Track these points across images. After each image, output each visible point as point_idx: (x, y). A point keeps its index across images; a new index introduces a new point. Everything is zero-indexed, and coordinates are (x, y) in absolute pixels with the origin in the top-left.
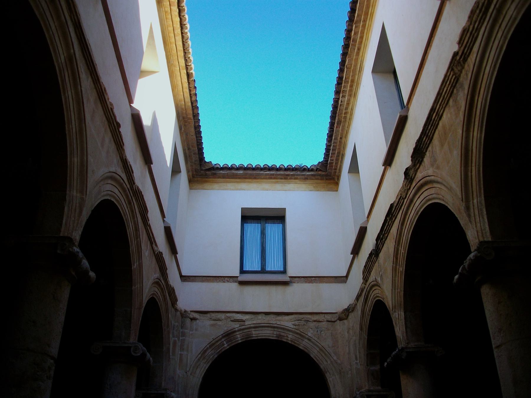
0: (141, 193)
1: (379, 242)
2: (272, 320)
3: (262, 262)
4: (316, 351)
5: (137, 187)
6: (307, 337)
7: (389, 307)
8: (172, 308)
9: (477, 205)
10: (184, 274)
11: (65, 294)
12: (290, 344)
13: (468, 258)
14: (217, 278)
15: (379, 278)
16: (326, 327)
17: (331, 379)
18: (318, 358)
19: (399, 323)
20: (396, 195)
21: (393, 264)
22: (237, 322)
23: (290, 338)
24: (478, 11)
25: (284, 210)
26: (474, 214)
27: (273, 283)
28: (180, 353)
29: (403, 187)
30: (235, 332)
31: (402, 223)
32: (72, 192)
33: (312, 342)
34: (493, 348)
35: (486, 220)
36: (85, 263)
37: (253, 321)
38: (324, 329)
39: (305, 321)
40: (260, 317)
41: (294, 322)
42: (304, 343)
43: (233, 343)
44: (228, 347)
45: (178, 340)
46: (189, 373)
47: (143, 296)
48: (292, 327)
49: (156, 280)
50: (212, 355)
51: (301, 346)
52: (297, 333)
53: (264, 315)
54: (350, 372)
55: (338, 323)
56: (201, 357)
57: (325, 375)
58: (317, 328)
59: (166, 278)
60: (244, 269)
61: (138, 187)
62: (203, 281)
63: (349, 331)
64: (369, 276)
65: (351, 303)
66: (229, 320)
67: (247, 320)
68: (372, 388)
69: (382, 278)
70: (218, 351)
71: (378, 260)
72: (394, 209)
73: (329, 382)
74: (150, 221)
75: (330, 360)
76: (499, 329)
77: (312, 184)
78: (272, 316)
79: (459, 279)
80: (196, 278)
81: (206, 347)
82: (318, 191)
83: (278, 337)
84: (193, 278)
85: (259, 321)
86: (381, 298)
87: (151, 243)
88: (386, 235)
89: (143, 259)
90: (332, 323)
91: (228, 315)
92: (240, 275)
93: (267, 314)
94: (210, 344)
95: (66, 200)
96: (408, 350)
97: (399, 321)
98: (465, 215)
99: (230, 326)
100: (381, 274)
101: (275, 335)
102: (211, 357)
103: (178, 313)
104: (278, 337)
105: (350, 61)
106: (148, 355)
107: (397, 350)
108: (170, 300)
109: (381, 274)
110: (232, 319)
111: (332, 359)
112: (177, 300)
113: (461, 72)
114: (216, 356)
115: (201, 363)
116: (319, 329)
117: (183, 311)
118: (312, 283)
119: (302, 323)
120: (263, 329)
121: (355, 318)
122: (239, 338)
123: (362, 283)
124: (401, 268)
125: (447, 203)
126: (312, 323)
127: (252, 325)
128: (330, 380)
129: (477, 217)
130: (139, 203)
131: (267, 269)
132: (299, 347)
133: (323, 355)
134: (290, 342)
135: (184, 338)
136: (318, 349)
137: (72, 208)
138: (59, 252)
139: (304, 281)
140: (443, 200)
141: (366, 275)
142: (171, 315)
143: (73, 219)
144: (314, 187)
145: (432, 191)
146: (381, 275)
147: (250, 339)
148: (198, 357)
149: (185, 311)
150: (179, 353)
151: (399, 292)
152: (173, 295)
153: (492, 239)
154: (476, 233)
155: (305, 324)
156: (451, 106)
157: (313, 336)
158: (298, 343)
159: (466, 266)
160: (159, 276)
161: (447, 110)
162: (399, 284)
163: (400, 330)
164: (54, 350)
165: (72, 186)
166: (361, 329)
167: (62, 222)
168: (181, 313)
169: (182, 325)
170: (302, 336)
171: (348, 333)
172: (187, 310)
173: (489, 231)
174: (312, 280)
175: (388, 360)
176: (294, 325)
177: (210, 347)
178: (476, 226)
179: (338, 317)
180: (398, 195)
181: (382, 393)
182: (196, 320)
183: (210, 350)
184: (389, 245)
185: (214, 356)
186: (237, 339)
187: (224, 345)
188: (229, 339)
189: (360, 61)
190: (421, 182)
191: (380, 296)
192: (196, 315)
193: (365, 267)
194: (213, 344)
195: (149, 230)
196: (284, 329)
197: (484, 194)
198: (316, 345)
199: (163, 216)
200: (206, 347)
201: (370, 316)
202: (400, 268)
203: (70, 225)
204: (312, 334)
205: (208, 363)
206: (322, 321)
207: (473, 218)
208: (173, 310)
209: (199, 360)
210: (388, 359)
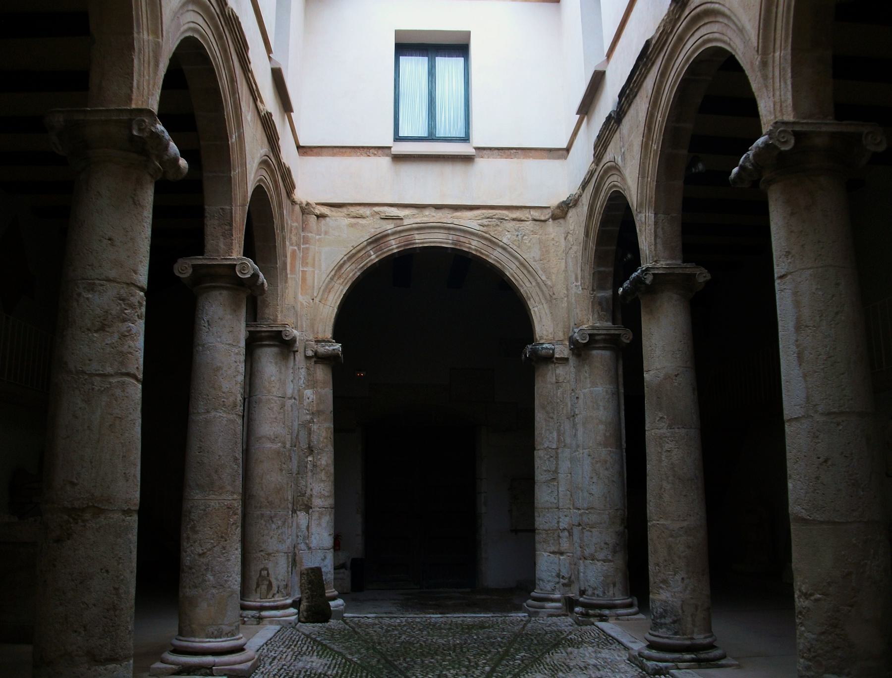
0: (236, 19)
1: (624, 99)
2: (446, 217)
3: (430, 123)
5: (230, 10)
6: (501, 244)
7: (632, 205)
8: (288, 201)
9: (778, 61)
10: (301, 144)
11: (148, 197)
12: (474, 254)
13: (755, 145)
14: (356, 150)
15: (620, 157)
17: (536, 309)
18: (517, 278)
19: (645, 230)
20: (657, 27)
21: (643, 137)
22: (391, 221)
23: (473, 245)
25: (468, 34)
26: (773, 75)
27: (448, 158)
28: (302, 269)
29: (668, 14)
30: (387, 235)
31: (663, 74)
32: (142, 34)
33: (509, 253)
34: (775, 278)
35: (790, 87)
36: (173, 148)
39: (499, 219)
40: (427, 212)
41: (480, 221)
43: (385, 253)
44: (377, 260)
45: (299, 250)
46: (317, 300)
47: (248, 185)
48: (478, 228)
49: (263, 158)
50: (352, 272)
53: (433, 210)
54: (566, 299)
56: (335, 274)
57: (527, 303)
59: (278, 153)
60: (401, 134)
61: (232, 10)
62: (334, 155)
63: (567, 236)
64: (603, 153)
65: (572, 193)
66: (378, 217)
67: (407, 216)
68: (597, 325)
69: (624, 157)
70: (361, 265)
71: (620, 129)
72: (650, 50)
73: (532, 313)
74: (252, 64)
75: (536, 280)
76: (786, 252)
79: (738, 173)
80: (323, 150)
81: (343, 260)
84: (319, 150)
85: (425, 219)
86: (621, 189)
87: (255, 100)
88: (636, 90)
89: (244, 125)
90: (542, 223)
91: (376, 209)
92: (393, 144)
94: (348, 256)
95: (134, 49)
96: (656, 272)
97: (645, 227)
98: (759, 74)
99: (379, 226)
100: (623, 151)
102: (351, 275)
103: (297, 208)
104: (456, 244)
106: (261, 274)
107: (639, 271)
108: (284, 188)
109: (623, 151)
110: (383, 215)
111: (539, 279)
112: (294, 187)
114: (359, 274)
115: (336, 284)
117: (304, 203)
118: (512, 158)
119: (494, 222)
120: (433, 231)
121: (577, 219)
122: (394, 246)
123: (591, 163)
124: (655, 144)
125: (735, 51)
126: (509, 222)
127: (414, 226)
128: (534, 310)
129: (777, 80)
130: (234, 34)
131: (438, 134)
133: (525, 272)
134: (474, 252)
135: (307, 246)
136: (517, 264)
137: (144, 61)
138: (135, 133)
139: (499, 155)
140: (729, 45)
141: (600, 150)
142: (286, 210)
143: (147, 77)
145: (715, 28)
146: (624, 153)
147: (411, 247)
148: (330, 276)
149: (308, 204)
150: (301, 269)
151: (649, 182)
152: (288, 180)
153: (794, 118)
154: (772, 106)
155: (499, 223)
157: (510, 243)
158: (486, 253)
159: (751, 156)
160: (268, 151)
162: (650, 170)
163: (645, 241)
164: (143, 279)
165: (141, 24)
166: (587, 234)
167: (132, 84)
168: (301, 207)
169: (303, 226)
170: (493, 243)
171: (565, 239)
172: (310, 202)
173: (791, 105)
175: (625, 285)
176: (481, 225)
177: (350, 258)
178: (773, 95)
179: (550, 214)
180: (659, 27)
181: (613, 332)
182: (326, 217)
183: (349, 264)
184: (640, 107)
185: (354, 275)
186: (391, 248)
187: (371, 256)
188: (379, 247)
190: (698, 10)
191: (619, 185)
192: (325, 210)
193: (599, 137)
194: (354, 255)
195: (251, 78)
197: (792, 46)
199: (269, 50)
200: (343, 260)
201: (601, 215)
202: (653, 145)
203: (144, 88)
204: (509, 239)
205: (346, 284)
206: (526, 219)
207: (771, 81)
208: (289, 202)
209: (332, 279)
210: (625, 283)
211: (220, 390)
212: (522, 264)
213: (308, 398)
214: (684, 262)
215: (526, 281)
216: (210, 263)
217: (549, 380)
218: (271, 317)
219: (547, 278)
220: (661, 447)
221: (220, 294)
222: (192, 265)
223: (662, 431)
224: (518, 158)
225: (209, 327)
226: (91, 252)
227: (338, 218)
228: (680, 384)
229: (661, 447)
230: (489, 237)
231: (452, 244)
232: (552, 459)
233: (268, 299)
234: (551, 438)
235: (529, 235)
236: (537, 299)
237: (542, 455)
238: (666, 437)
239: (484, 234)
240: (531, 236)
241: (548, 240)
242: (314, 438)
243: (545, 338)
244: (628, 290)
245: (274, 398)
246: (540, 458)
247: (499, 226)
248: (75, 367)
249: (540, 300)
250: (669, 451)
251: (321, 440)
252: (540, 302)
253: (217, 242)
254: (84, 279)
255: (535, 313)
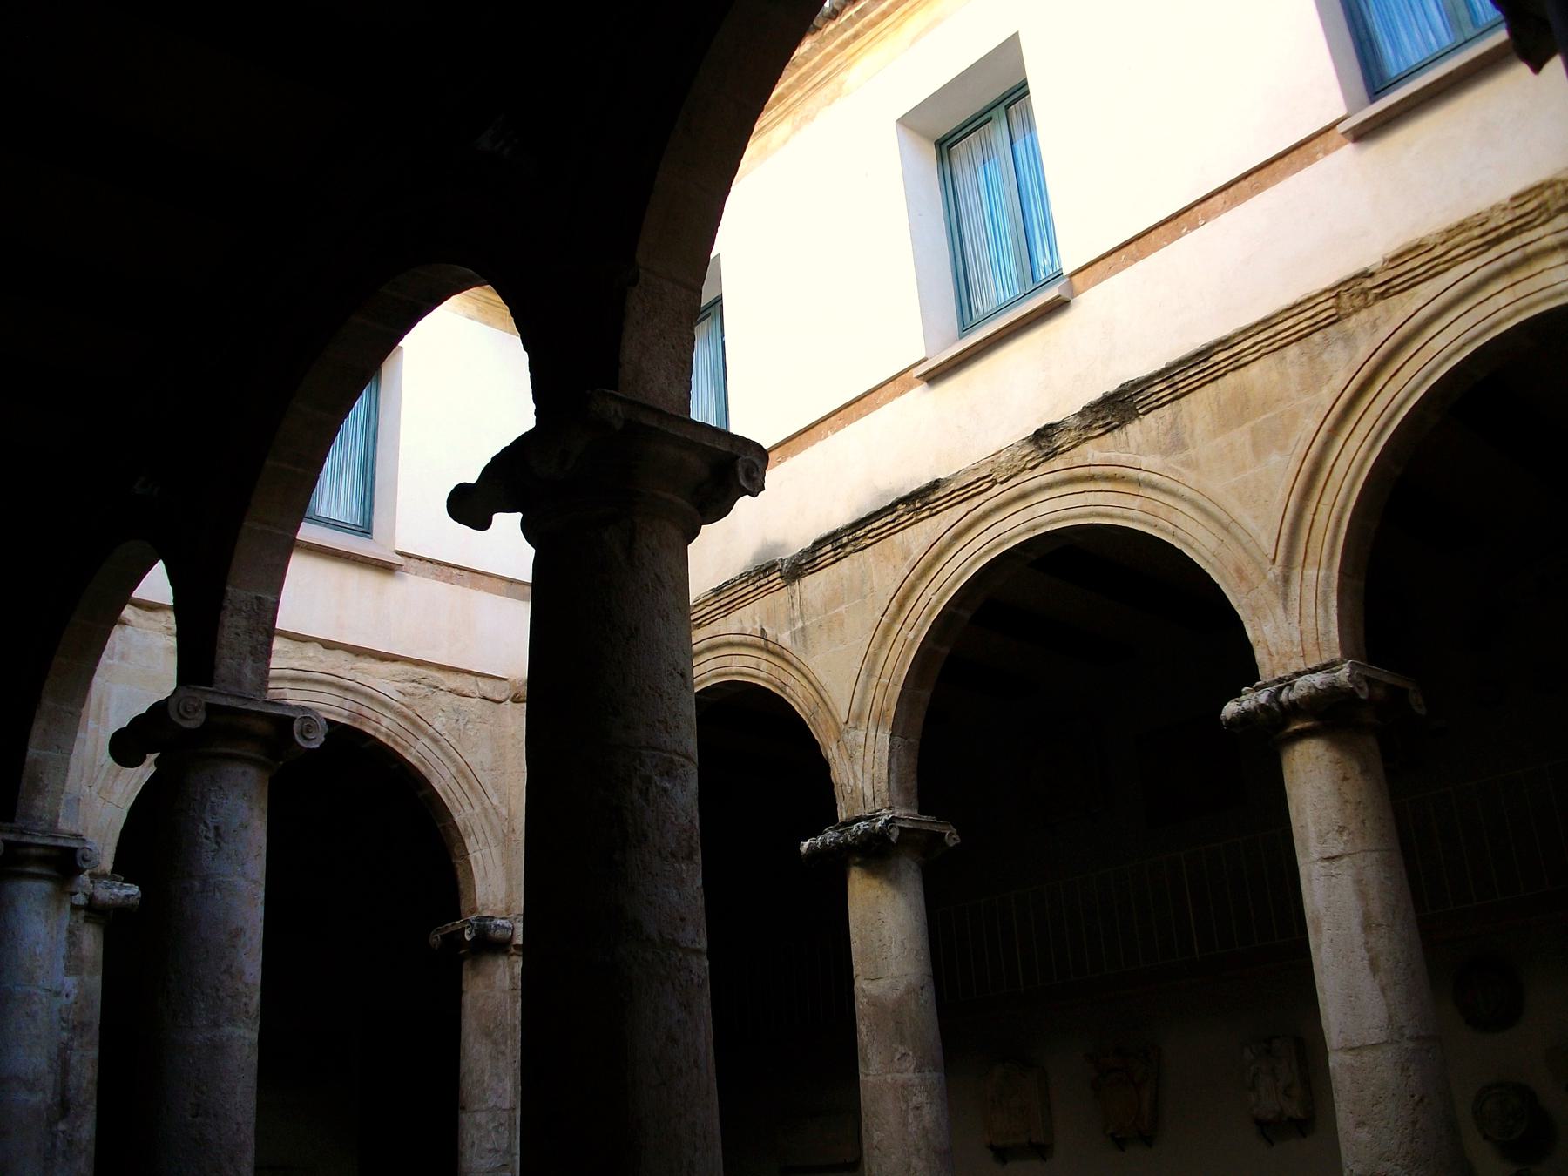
4: (448, 776)
6: (430, 730)
16: (479, 713)
17: (478, 855)
18: (452, 796)
23: (383, 727)
24: (1476, 232)
33: (441, 748)
37: (290, 658)
38: (474, 716)
39: (430, 686)
42: (419, 746)
51: (411, 754)
52: (406, 717)
55: (509, 706)
58: (457, 711)
75: (482, 804)
77: (475, 298)
78: (343, 656)
82: (488, 324)
83: (354, 720)
93: (329, 645)
101: (346, 713)
104: (354, 720)
105: (813, 51)
111: (487, 802)
113: (1357, 311)
116: (462, 715)
119: (423, 690)
126: (445, 695)
132: (404, 755)
133: (466, 787)
134: (383, 739)
136: (453, 770)
144: (479, 310)
155: (430, 694)
156: (1288, 359)
158: (404, 743)
161: (1268, 361)
170: (417, 725)
174: (452, 573)
182: (126, 624)
189: (836, 63)
196: (372, 698)
198: (450, 757)
206: (471, 694)
211: (241, 979)
212: (461, 771)
213: (67, 996)
214: (921, 812)
215: (465, 802)
216: (244, 707)
217: (498, 983)
218: (47, 817)
219: (500, 803)
220: (907, 1102)
221: (244, 774)
222: (207, 704)
223: (905, 1076)
224: (463, 586)
225: (219, 840)
226: (661, 696)
227: (149, 631)
228: (926, 1002)
229: (907, 1102)
230: (413, 716)
231: (348, 717)
232: (502, 1129)
233: (45, 779)
234: (500, 1091)
235: (475, 722)
236: (481, 837)
237: (483, 1122)
238: (912, 1086)
239: (405, 709)
240: (479, 726)
241: (503, 737)
242: (72, 1080)
243: (490, 908)
244: (833, 847)
245: (39, 991)
246: (478, 1126)
247: (429, 699)
248: (660, 933)
249: (486, 838)
250: (918, 1108)
251: (84, 1085)
252: (487, 844)
253: (239, 664)
254: (654, 748)
255: (477, 862)
